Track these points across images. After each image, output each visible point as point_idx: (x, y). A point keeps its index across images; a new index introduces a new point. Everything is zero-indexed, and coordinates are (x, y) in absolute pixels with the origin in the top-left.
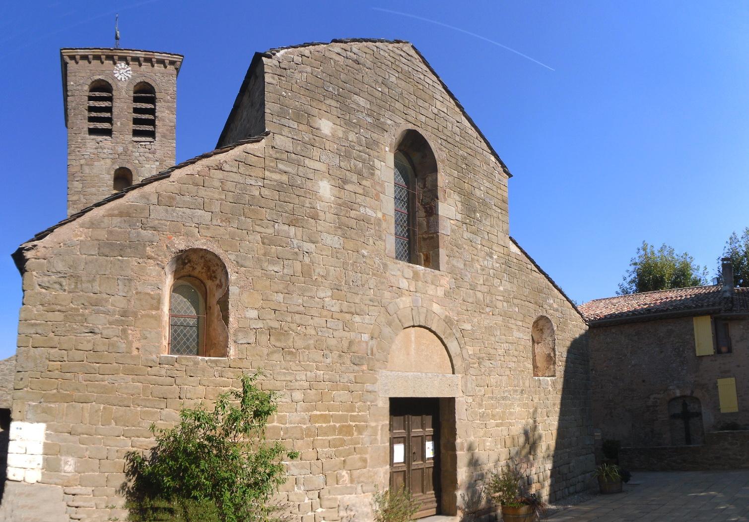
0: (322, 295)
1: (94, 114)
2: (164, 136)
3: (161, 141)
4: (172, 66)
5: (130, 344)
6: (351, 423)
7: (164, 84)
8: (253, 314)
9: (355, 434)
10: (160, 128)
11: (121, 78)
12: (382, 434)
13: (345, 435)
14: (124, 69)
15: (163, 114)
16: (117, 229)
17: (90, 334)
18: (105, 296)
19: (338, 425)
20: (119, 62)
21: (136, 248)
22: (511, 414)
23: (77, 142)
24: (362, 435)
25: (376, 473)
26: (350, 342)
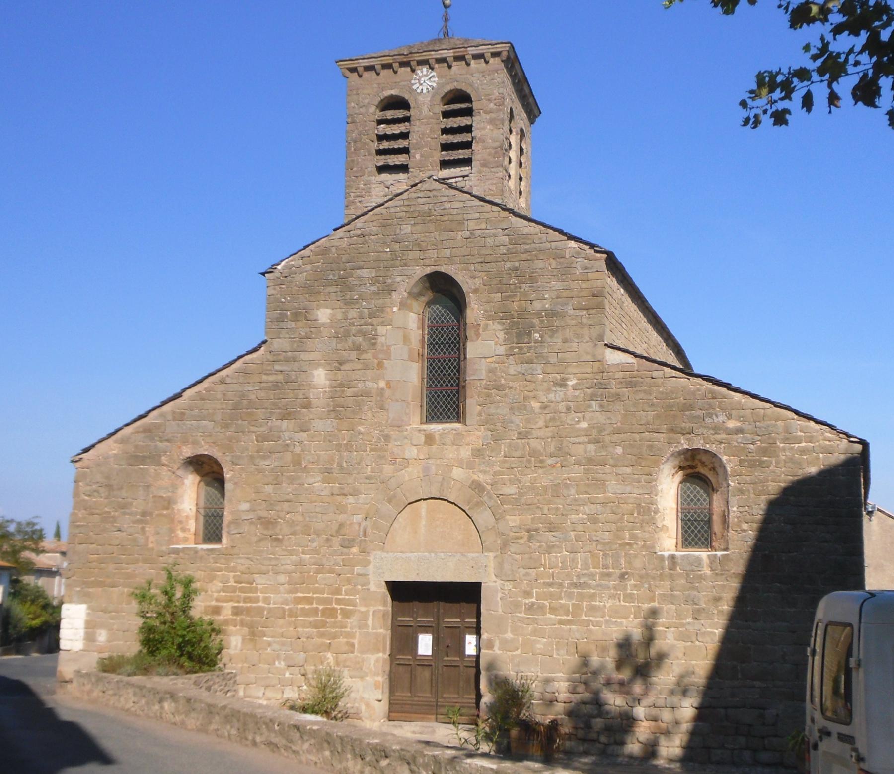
0: (311, 481)
1: (385, 145)
2: (484, 165)
3: (480, 173)
4: (497, 58)
5: (147, 538)
6: (336, 606)
7: (484, 87)
8: (245, 506)
9: (339, 617)
10: (479, 153)
11: (422, 90)
12: (373, 620)
13: (328, 618)
14: (427, 75)
15: (483, 132)
16: (141, 443)
17: (119, 532)
18: (130, 500)
19: (321, 607)
20: (420, 67)
21: (154, 458)
22: (593, 609)
23: (358, 188)
24: (349, 619)
25: (363, 660)
26: (340, 525)
